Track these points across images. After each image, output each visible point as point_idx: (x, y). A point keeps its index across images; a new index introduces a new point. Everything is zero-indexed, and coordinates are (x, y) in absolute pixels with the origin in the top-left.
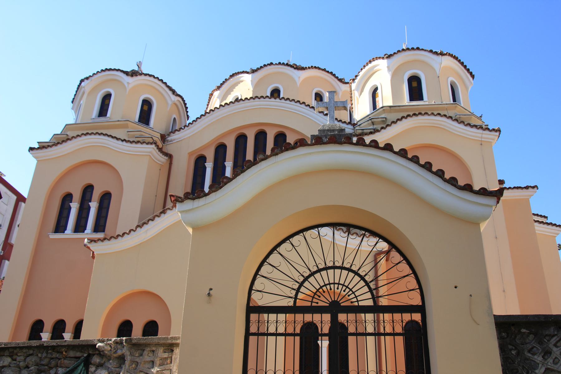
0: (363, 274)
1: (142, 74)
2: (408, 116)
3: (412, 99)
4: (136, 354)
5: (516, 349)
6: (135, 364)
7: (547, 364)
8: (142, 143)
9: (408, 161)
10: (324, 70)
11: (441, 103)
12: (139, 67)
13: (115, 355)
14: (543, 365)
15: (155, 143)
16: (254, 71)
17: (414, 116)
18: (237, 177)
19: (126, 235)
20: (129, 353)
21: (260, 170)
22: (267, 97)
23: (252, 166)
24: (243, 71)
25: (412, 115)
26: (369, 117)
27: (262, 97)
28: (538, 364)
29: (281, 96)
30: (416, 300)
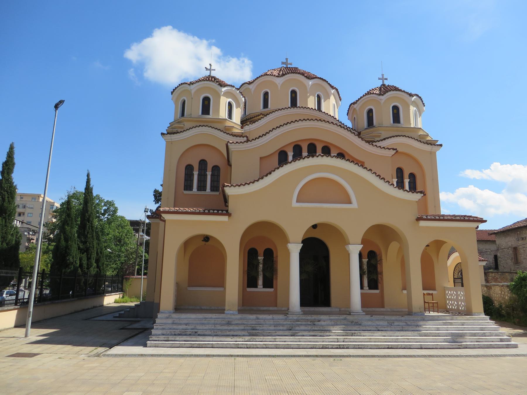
22: (289, 107)
24: (320, 78)
29: (298, 105)
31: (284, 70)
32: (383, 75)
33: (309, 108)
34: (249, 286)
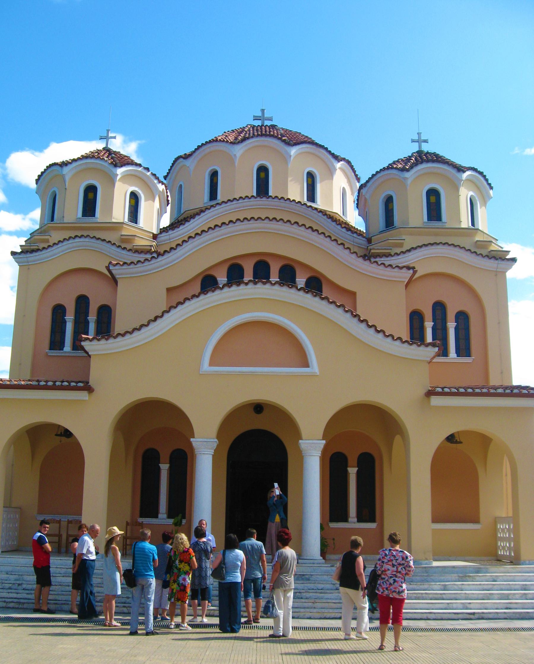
22: (253, 196)
31: (249, 130)
32: (419, 134)
33: (289, 199)
34: (332, 520)
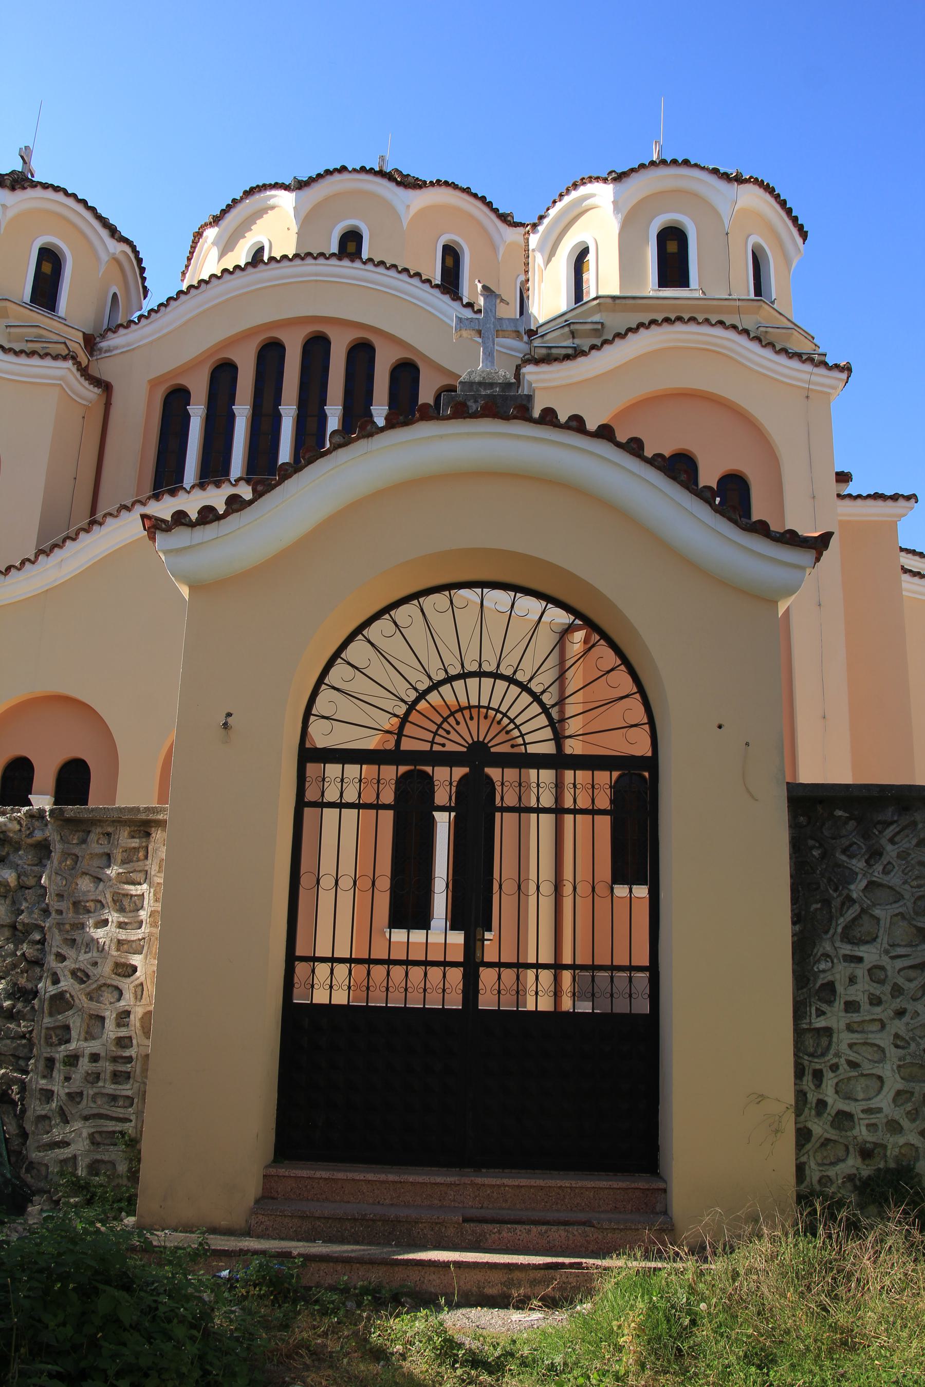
0: (537, 689)
1: (35, 185)
2: (653, 322)
3: (664, 281)
4: (73, 839)
5: (821, 846)
6: (72, 859)
7: (871, 874)
8: (42, 357)
9: (643, 464)
10: (467, 191)
11: (728, 297)
12: (25, 162)
13: (29, 841)
14: (864, 875)
15: (74, 358)
16: (303, 184)
17: (665, 324)
18: (286, 482)
19: (13, 571)
20: (59, 837)
21: (333, 469)
23: (318, 459)
24: (276, 184)
25: (662, 322)
26: (566, 317)
27: (322, 255)
28: (857, 874)
29: (365, 255)
30: (642, 748)
